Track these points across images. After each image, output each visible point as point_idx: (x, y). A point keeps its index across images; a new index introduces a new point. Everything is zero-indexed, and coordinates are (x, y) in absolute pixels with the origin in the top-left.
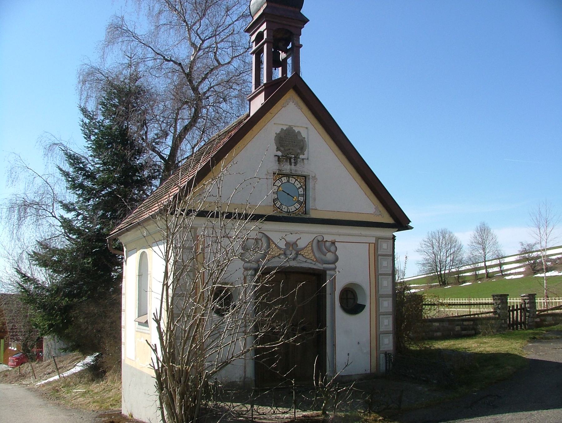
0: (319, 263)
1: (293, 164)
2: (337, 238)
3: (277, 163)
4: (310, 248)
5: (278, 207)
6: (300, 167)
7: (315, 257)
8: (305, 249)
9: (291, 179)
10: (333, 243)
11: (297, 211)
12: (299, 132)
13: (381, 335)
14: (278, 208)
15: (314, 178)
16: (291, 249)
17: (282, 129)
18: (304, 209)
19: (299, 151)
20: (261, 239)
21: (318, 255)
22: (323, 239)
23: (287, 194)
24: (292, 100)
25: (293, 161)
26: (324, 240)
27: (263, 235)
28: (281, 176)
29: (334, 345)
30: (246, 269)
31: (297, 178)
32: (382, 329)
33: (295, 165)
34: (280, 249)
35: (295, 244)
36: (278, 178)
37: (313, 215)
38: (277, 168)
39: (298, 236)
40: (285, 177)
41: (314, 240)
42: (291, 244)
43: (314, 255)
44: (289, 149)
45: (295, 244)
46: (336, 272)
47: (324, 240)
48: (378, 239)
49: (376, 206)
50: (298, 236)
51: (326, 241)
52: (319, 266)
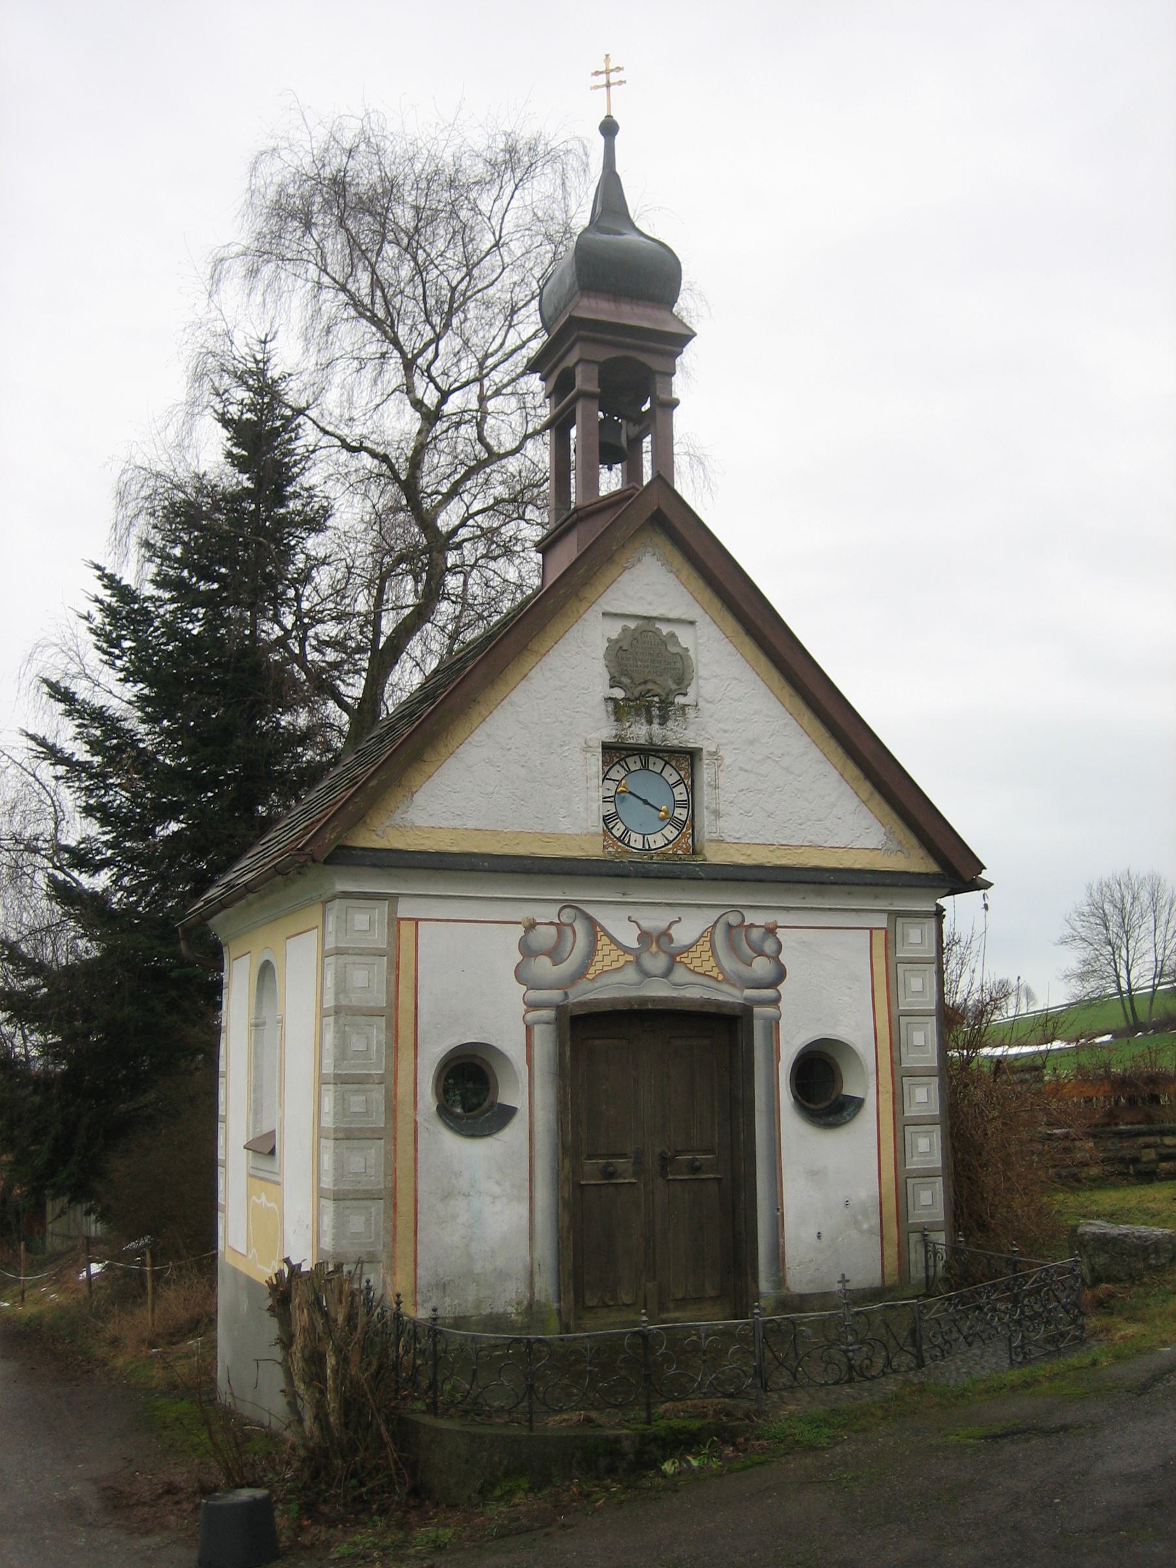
0: (733, 985)
3: (613, 718)
4: (707, 946)
7: (722, 972)
8: (693, 949)
11: (670, 846)
12: (672, 636)
14: (618, 839)
16: (654, 948)
18: (690, 841)
20: (571, 925)
21: (730, 964)
22: (743, 920)
23: (641, 802)
25: (655, 712)
28: (624, 752)
30: (532, 1006)
32: (914, 1163)
33: (659, 724)
34: (626, 950)
35: (665, 934)
36: (616, 760)
37: (714, 855)
38: (614, 732)
39: (671, 915)
42: (655, 934)
43: (718, 965)
45: (665, 934)
48: (895, 915)
52: (731, 995)
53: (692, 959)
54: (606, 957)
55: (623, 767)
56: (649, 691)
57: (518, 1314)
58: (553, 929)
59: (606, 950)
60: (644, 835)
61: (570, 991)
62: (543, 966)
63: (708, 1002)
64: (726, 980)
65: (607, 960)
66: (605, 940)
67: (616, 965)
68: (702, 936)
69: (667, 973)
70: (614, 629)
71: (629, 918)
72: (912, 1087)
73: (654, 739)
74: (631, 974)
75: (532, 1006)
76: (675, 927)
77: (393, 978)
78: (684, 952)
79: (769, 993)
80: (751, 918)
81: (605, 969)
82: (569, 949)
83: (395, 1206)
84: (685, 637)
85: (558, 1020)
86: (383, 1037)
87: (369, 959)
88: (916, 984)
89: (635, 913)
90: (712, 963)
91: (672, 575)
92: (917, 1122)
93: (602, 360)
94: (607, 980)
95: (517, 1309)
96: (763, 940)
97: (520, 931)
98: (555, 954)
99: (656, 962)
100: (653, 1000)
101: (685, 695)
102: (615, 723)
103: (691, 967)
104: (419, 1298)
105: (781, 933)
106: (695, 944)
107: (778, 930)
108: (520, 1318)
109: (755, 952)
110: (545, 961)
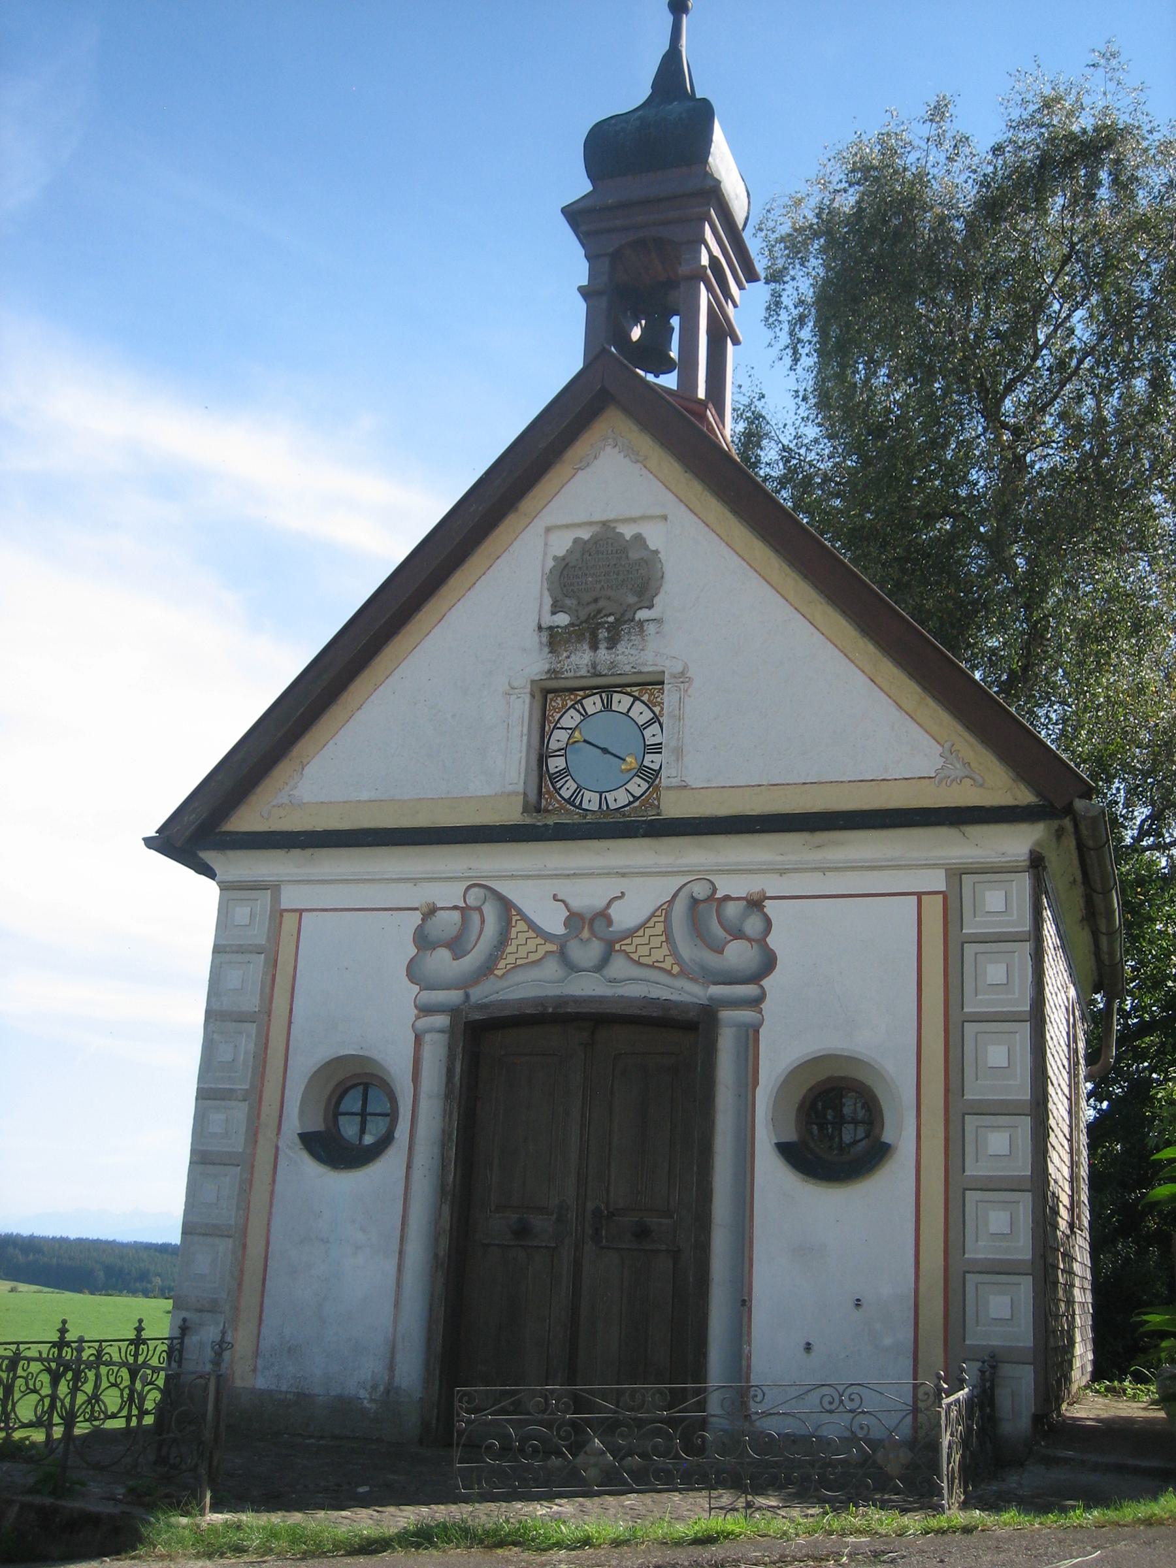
0: (694, 980)
1: (603, 645)
2: (772, 885)
3: (546, 650)
4: (660, 928)
5: (567, 797)
6: (627, 652)
7: (679, 960)
8: (640, 933)
9: (616, 697)
10: (755, 903)
11: (637, 804)
12: (639, 539)
13: (968, 1276)
14: (568, 801)
15: (683, 677)
16: (586, 934)
17: (576, 541)
19: (631, 599)
20: (479, 909)
21: (688, 950)
22: (715, 890)
24: (610, 441)
25: (603, 634)
26: (717, 896)
27: (489, 894)
28: (581, 693)
29: (743, 1303)
30: (425, 1010)
31: (641, 691)
32: (979, 1249)
33: (607, 648)
34: (547, 937)
35: (603, 915)
36: (570, 703)
37: (673, 807)
38: (547, 667)
39: (612, 887)
40: (598, 696)
41: (678, 900)
42: (589, 916)
43: (674, 953)
44: (596, 600)
45: (603, 915)
46: (760, 1012)
47: (717, 896)
48: (956, 874)
49: (947, 745)
50: (612, 887)
51: (727, 898)
52: (691, 993)
53: (639, 947)
54: (522, 946)
55: (578, 711)
56: (599, 611)
57: (372, 1400)
58: (456, 915)
59: (522, 938)
60: (601, 794)
61: (471, 991)
62: (441, 961)
63: (654, 1002)
64: (683, 973)
65: (522, 952)
66: (522, 926)
67: (533, 957)
68: (653, 915)
69: (601, 966)
70: (561, 544)
71: (555, 896)
72: (980, 1130)
73: (598, 668)
74: (552, 969)
75: (425, 1010)
76: (616, 904)
77: (269, 978)
78: (628, 937)
79: (748, 990)
80: (726, 886)
81: (519, 962)
82: (474, 938)
83: (244, 1246)
84: (655, 538)
85: (452, 1030)
86: (251, 1047)
87: (247, 957)
88: (995, 972)
89: (564, 888)
90: (665, 950)
91: (639, 465)
92: (989, 1185)
93: (611, 250)
94: (520, 976)
95: (370, 1394)
96: (744, 917)
97: (416, 918)
98: (456, 945)
99: (587, 952)
100: (577, 1000)
101: (650, 607)
102: (550, 655)
103: (635, 956)
104: (260, 1362)
105: (770, 907)
106: (643, 925)
107: (767, 903)
108: (373, 1406)
109: (730, 935)
110: (444, 954)
